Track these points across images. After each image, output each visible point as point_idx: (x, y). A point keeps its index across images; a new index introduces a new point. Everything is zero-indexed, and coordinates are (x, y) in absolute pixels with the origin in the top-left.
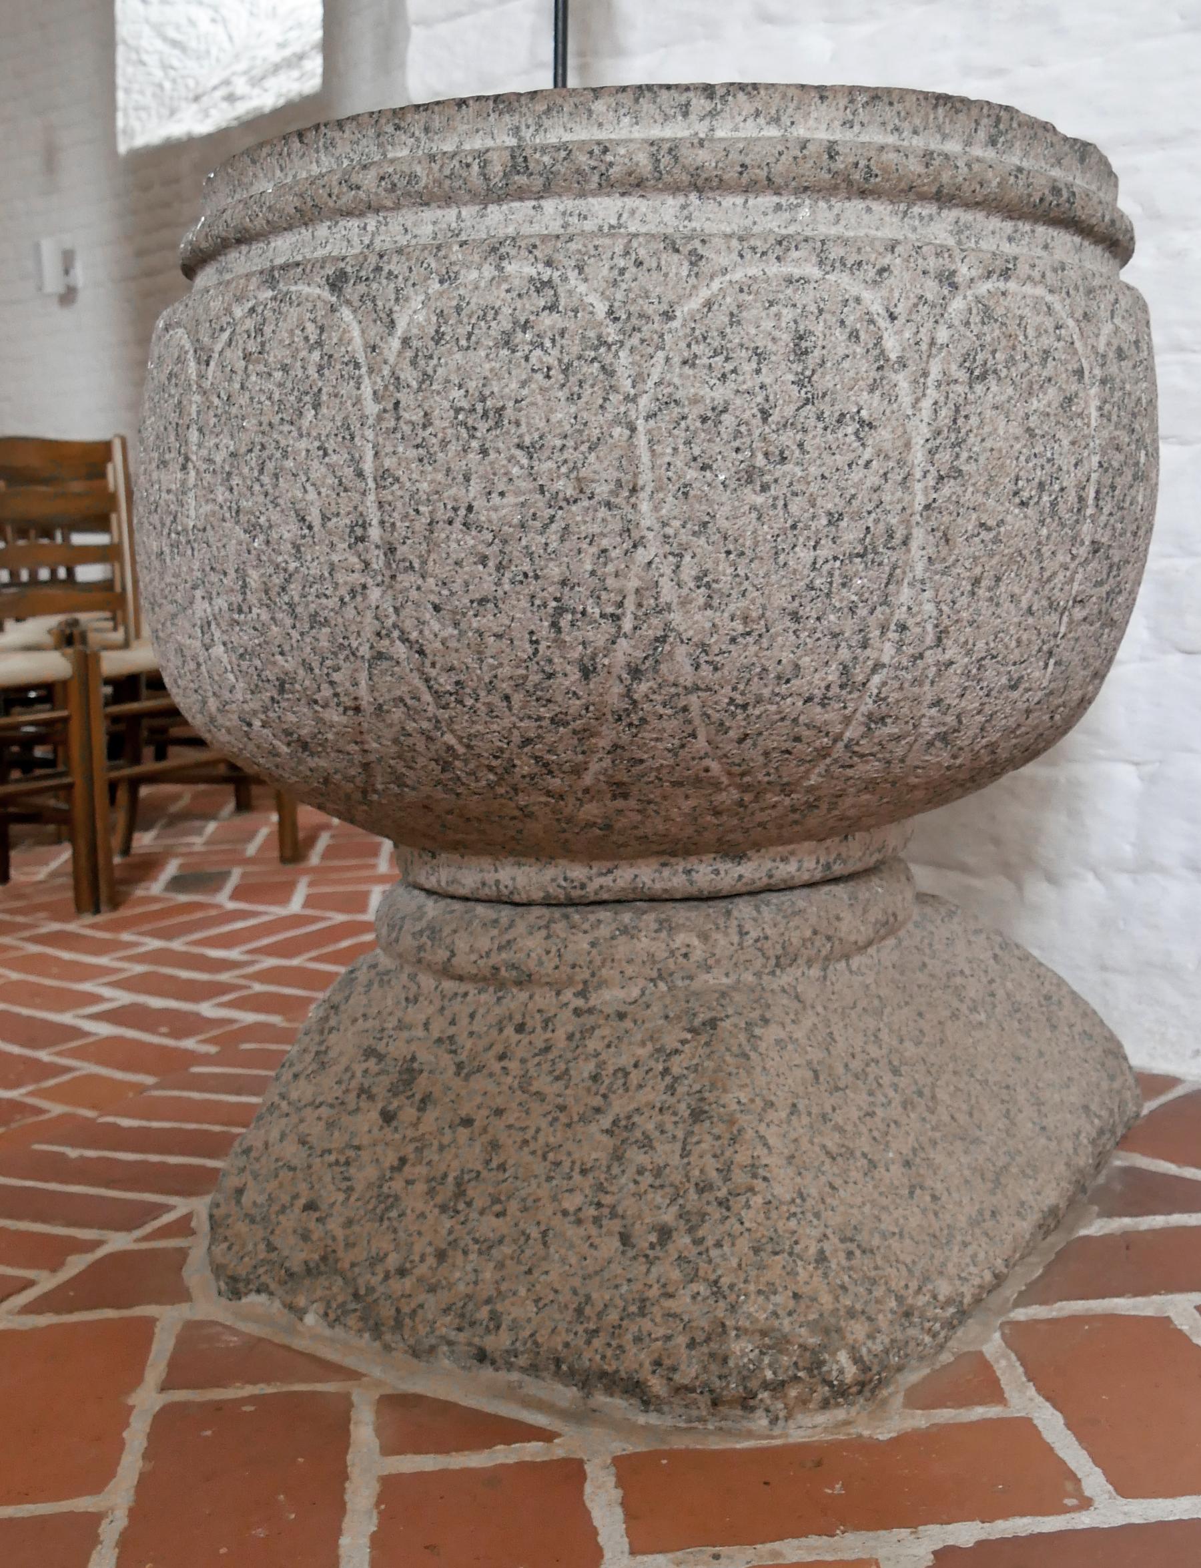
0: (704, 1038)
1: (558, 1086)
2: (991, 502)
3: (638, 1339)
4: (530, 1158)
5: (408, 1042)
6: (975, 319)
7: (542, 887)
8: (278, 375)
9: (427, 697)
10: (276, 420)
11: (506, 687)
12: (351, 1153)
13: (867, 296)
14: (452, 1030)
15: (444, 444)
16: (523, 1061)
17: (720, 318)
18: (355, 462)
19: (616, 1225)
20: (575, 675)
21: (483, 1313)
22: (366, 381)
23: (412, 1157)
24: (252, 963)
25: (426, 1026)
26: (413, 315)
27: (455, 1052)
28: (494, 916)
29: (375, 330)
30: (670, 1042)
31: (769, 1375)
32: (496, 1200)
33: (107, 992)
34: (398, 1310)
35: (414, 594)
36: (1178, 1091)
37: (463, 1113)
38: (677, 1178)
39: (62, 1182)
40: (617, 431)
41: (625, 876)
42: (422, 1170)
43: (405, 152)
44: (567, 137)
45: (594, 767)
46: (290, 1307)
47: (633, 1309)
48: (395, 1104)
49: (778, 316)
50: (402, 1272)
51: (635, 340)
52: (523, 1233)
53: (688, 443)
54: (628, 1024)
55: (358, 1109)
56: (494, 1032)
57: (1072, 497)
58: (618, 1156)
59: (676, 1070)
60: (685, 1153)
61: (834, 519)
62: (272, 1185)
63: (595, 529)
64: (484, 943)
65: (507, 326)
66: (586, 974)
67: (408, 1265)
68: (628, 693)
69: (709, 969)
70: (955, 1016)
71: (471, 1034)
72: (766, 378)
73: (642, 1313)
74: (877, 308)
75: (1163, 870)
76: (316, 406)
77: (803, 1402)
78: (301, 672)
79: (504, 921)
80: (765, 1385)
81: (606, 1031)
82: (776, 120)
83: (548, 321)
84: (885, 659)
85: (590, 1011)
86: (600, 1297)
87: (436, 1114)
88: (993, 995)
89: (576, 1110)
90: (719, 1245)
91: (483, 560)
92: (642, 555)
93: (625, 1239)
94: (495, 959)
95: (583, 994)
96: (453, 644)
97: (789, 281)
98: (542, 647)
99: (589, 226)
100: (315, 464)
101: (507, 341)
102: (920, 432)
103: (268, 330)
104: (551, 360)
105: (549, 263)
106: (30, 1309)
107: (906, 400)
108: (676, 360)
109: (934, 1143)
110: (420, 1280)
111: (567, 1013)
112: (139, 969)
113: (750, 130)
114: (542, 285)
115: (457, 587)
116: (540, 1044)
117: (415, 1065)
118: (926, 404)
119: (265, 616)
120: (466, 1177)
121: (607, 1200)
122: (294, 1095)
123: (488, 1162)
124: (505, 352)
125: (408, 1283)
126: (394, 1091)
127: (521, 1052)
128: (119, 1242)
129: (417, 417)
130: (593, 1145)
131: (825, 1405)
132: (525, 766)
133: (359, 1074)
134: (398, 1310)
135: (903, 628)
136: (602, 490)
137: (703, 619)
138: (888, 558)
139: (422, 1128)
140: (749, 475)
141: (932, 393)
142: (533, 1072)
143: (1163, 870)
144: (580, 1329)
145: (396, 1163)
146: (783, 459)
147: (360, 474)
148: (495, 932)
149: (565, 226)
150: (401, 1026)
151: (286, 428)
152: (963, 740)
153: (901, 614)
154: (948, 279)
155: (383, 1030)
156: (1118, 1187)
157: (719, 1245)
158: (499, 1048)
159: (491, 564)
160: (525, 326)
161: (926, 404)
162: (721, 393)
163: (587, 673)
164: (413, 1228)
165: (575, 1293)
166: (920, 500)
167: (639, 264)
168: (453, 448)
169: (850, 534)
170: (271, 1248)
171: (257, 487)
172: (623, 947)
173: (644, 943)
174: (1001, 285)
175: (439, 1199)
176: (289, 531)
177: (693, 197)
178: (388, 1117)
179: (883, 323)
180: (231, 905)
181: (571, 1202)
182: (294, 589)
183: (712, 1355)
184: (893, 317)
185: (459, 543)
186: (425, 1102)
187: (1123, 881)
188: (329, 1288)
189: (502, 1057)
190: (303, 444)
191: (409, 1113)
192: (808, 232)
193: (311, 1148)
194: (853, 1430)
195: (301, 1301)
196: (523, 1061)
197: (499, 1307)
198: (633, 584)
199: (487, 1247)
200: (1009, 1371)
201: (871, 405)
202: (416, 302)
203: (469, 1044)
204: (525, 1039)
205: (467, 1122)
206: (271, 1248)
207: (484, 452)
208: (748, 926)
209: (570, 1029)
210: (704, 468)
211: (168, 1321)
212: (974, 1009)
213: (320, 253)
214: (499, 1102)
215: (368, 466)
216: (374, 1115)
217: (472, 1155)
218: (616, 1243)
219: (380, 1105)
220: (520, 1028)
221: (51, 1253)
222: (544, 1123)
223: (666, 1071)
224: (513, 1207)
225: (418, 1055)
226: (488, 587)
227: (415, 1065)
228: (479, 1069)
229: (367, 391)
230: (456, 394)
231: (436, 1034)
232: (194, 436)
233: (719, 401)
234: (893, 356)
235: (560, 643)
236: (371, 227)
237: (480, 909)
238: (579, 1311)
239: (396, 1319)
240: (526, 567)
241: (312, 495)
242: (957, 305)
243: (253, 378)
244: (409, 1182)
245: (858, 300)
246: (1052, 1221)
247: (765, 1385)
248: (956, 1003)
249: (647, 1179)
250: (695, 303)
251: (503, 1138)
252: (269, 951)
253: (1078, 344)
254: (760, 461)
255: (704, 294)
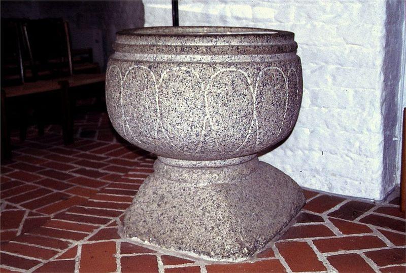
0: (219, 193)
2: (268, 106)
3: (209, 246)
5: (162, 192)
6: (264, 75)
7: (187, 165)
8: (139, 82)
9: (168, 138)
11: (183, 137)
12: (152, 212)
13: (245, 73)
14: (171, 190)
15: (171, 98)
16: (185, 196)
17: (219, 78)
18: (155, 99)
20: (195, 136)
21: (180, 241)
22: (156, 85)
24: (108, 158)
25: (166, 188)
26: (164, 75)
29: (157, 77)
30: (213, 194)
31: (232, 252)
32: (181, 221)
33: (75, 165)
35: (166, 121)
36: (318, 196)
37: (174, 205)
38: (215, 218)
39: (91, 214)
40: (201, 97)
41: (203, 163)
42: (166, 215)
43: (161, 44)
44: (191, 45)
45: (198, 149)
46: (142, 239)
47: (208, 241)
48: (160, 203)
49: (229, 78)
50: (163, 234)
51: (204, 82)
53: (214, 99)
54: (204, 190)
56: (179, 191)
57: (283, 102)
58: (204, 214)
59: (214, 199)
60: (216, 214)
61: (239, 111)
62: (136, 217)
63: (198, 113)
64: (177, 175)
65: (181, 78)
66: (196, 181)
68: (204, 139)
69: (219, 180)
70: (267, 186)
72: (227, 88)
73: (209, 241)
74: (246, 75)
75: (314, 150)
76: (147, 89)
77: (239, 256)
78: (144, 132)
79: (181, 171)
80: (231, 254)
82: (228, 42)
83: (189, 78)
84: (249, 132)
88: (275, 181)
89: (195, 205)
90: (223, 230)
91: (178, 117)
92: (206, 117)
93: (206, 229)
94: (179, 178)
96: (173, 130)
97: (231, 71)
98: (189, 131)
99: (195, 60)
101: (181, 81)
102: (254, 96)
103: (137, 73)
104: (189, 85)
105: (189, 68)
106: (90, 240)
107: (252, 90)
108: (211, 86)
109: (262, 211)
112: (80, 159)
113: (223, 44)
114: (188, 72)
115: (174, 121)
116: (188, 193)
118: (255, 91)
119: (137, 122)
121: (202, 222)
122: (139, 200)
124: (181, 83)
125: (165, 236)
126: (160, 200)
128: (103, 227)
129: (166, 93)
130: (199, 212)
131: (242, 257)
132: (186, 149)
135: (252, 127)
136: (199, 107)
137: (217, 128)
138: (249, 117)
139: (166, 208)
140: (224, 104)
141: (256, 89)
143: (314, 150)
146: (230, 102)
147: (156, 101)
149: (191, 60)
150: (160, 188)
152: (264, 143)
153: (252, 125)
154: (259, 69)
156: (301, 217)
157: (223, 230)
158: (180, 193)
159: (180, 118)
160: (185, 79)
161: (255, 91)
162: (219, 91)
163: (197, 136)
164: (165, 226)
165: (197, 238)
166: (255, 107)
167: (204, 69)
168: (173, 98)
169: (243, 113)
172: (203, 177)
173: (207, 176)
174: (269, 68)
175: (170, 221)
176: (142, 109)
177: (213, 56)
178: (159, 205)
179: (248, 78)
180: (98, 141)
182: (143, 118)
183: (222, 249)
184: (249, 77)
185: (174, 114)
187: (307, 152)
189: (181, 195)
192: (234, 62)
194: (247, 261)
195: (144, 239)
197: (183, 240)
198: (205, 122)
199: (180, 230)
200: (276, 251)
201: (246, 92)
202: (165, 72)
204: (185, 192)
205: (175, 207)
207: (178, 100)
208: (226, 173)
210: (217, 103)
211: (118, 242)
212: (271, 185)
213: (145, 59)
214: (181, 203)
218: (204, 230)
220: (184, 190)
221: (90, 229)
222: (189, 207)
223: (212, 199)
224: (185, 222)
226: (179, 121)
229: (156, 87)
230: (173, 89)
232: (122, 88)
233: (219, 92)
234: (249, 83)
235: (192, 131)
236: (155, 56)
237: (176, 168)
238: (198, 241)
239: (163, 242)
240: (186, 118)
241: (146, 103)
242: (261, 73)
245: (243, 74)
246: (286, 224)
247: (231, 254)
248: (267, 184)
250: (215, 76)
252: (111, 154)
253: (284, 76)
254: (226, 102)
255: (216, 74)
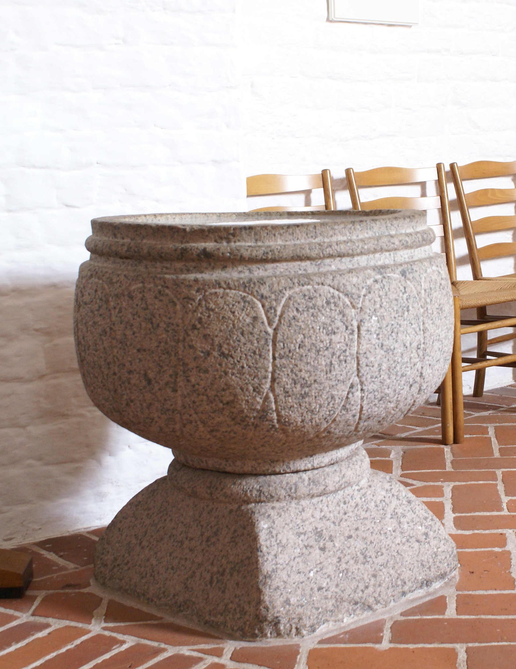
1: (368, 514)
4: (376, 536)
10: (397, 316)
14: (323, 514)
16: (353, 512)
19: (414, 539)
23: (341, 555)
27: (328, 520)
28: (334, 469)
34: (375, 597)
37: (346, 535)
42: (347, 558)
50: (367, 587)
52: (392, 556)
55: (310, 553)
56: (338, 508)
59: (396, 494)
64: (337, 479)
67: (367, 584)
71: (330, 512)
73: (436, 556)
76: (408, 311)
81: (369, 492)
85: (361, 489)
86: (425, 558)
87: (338, 540)
93: (418, 541)
95: (357, 485)
100: (409, 328)
110: (374, 585)
111: (356, 493)
116: (354, 505)
117: (319, 530)
120: (364, 551)
123: (366, 543)
125: (371, 589)
127: (350, 509)
133: (300, 542)
134: (375, 597)
142: (358, 513)
144: (426, 569)
145: (338, 560)
148: (338, 474)
151: (400, 318)
155: (298, 525)
158: (342, 512)
165: (418, 561)
170: (317, 609)
171: (390, 338)
178: (323, 549)
181: (398, 540)
186: (331, 539)
188: (345, 607)
190: (405, 322)
191: (329, 545)
193: (303, 573)
196: (353, 512)
197: (402, 578)
199: (385, 565)
203: (332, 515)
205: (350, 537)
206: (317, 609)
209: (359, 496)
214: (355, 526)
215: (422, 328)
216: (318, 551)
217: (360, 545)
219: (317, 547)
220: (345, 503)
223: (393, 495)
224: (384, 550)
225: (317, 526)
227: (319, 530)
228: (341, 520)
231: (318, 517)
238: (422, 565)
243: (385, 303)
244: (347, 563)
249: (411, 524)
251: (364, 535)
